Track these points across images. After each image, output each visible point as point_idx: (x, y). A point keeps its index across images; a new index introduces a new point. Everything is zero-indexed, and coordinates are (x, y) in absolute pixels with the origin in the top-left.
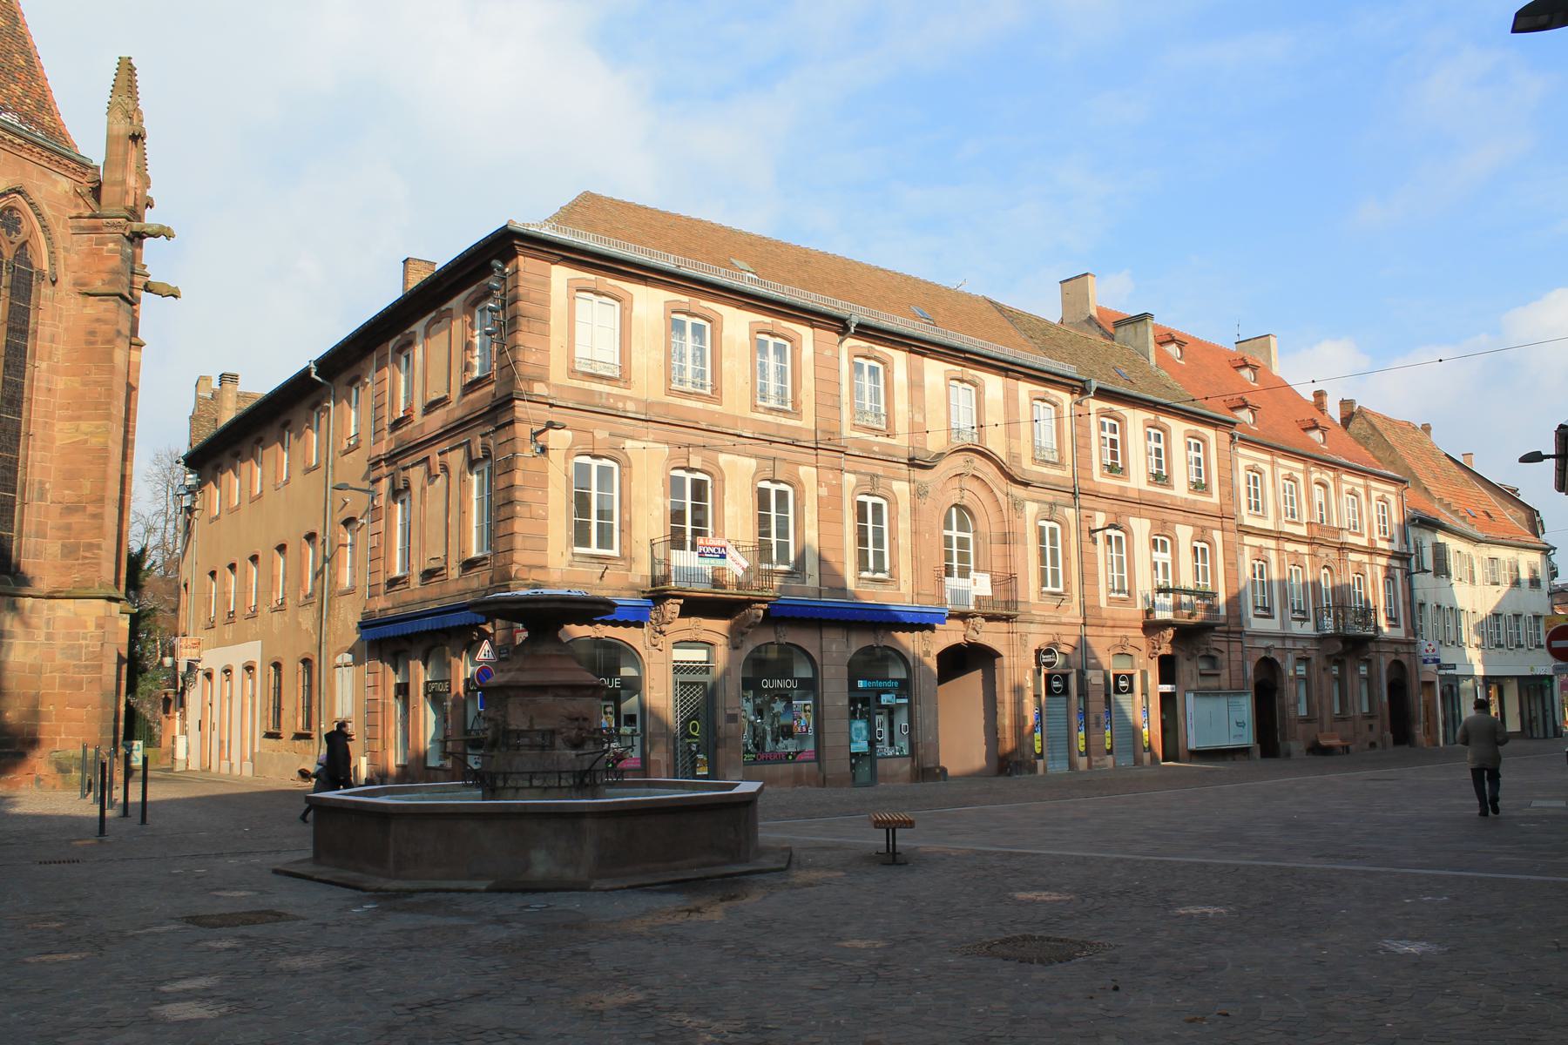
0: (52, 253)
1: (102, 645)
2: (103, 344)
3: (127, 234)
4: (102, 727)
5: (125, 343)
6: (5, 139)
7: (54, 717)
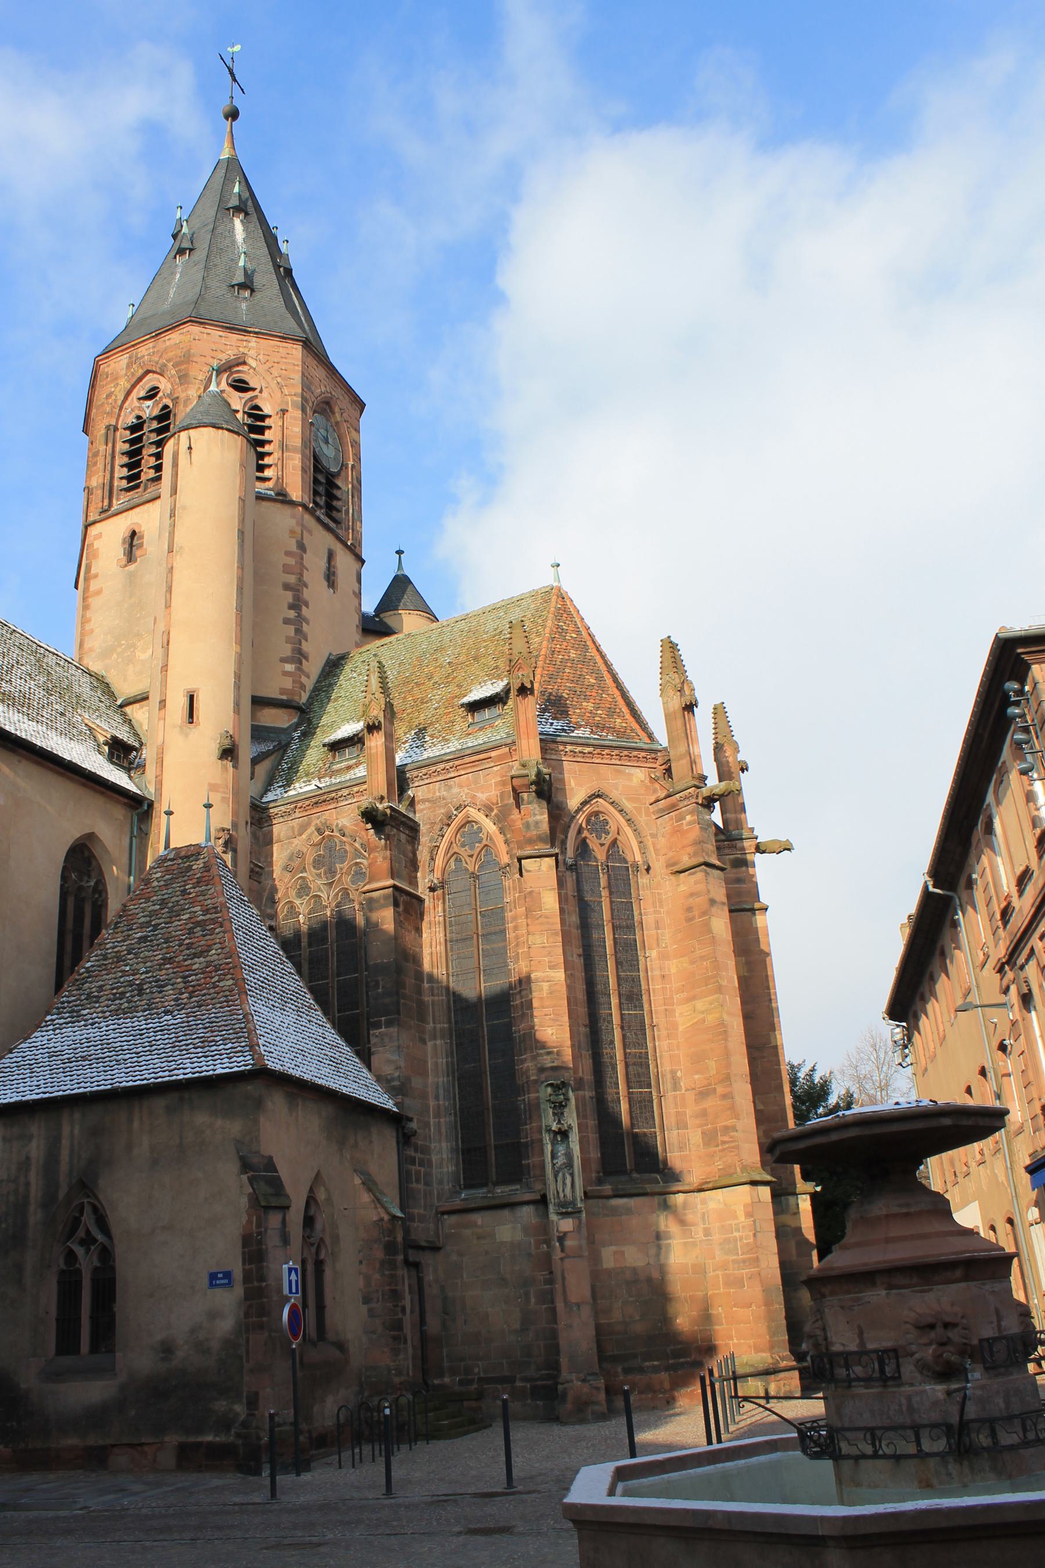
0: (641, 842)
1: (755, 1235)
2: (700, 917)
3: (700, 802)
4: (769, 1328)
5: (722, 910)
6: (575, 752)
7: (724, 1321)
